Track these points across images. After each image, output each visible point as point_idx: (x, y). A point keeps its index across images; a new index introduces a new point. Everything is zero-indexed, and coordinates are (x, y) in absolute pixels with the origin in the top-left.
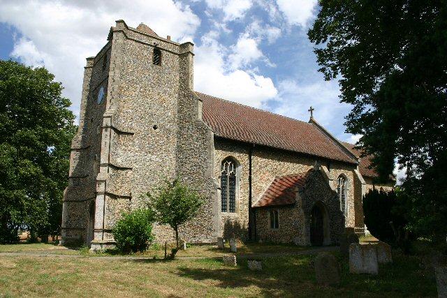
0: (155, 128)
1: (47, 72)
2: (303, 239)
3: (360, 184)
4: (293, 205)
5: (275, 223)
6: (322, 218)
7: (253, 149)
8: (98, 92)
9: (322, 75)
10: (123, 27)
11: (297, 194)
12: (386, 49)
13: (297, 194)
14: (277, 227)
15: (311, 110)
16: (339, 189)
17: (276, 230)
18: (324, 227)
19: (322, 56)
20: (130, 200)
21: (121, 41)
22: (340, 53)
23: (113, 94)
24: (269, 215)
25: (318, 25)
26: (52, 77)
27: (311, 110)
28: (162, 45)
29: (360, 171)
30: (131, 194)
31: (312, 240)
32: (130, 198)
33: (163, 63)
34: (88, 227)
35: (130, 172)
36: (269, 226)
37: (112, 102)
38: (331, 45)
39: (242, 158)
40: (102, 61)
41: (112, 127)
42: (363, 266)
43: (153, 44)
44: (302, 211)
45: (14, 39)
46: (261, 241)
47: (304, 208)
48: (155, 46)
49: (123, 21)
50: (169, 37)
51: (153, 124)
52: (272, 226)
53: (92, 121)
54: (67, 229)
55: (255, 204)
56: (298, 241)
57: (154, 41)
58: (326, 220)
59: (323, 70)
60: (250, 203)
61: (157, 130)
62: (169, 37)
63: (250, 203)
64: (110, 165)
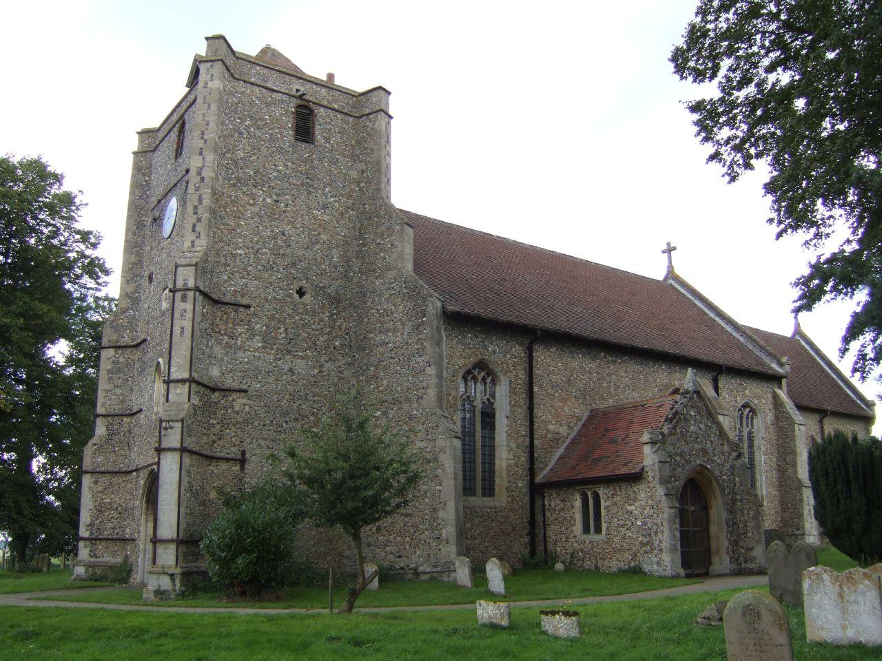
0: (301, 293)
1: (45, 167)
2: (664, 558)
3: (792, 423)
4: (636, 477)
5: (592, 521)
6: (706, 508)
7: (533, 336)
8: (163, 210)
9: (717, 168)
10: (224, 51)
11: (647, 449)
12: (709, 30)
13: (647, 449)
14: (598, 530)
15: (670, 250)
16: (741, 437)
17: (596, 538)
18: (713, 529)
19: (708, 117)
20: (242, 468)
21: (216, 84)
22: (752, 104)
23: (200, 211)
24: (578, 503)
25: (695, 35)
26: (58, 178)
27: (670, 250)
28: (312, 94)
29: (790, 394)
30: (243, 453)
31: (685, 563)
32: (243, 462)
33: (319, 137)
34: (142, 534)
35: (241, 401)
36: (578, 528)
37: (198, 229)
38: (727, 89)
39: (505, 354)
40: (174, 135)
41: (197, 289)
42: (844, 628)
43: (294, 92)
44: (660, 491)
45: (698, 379)
46: (559, 566)
47: (664, 481)
48: (301, 97)
49: (223, 38)
50: (331, 76)
51: (296, 286)
52: (586, 530)
53: (150, 279)
54: (93, 540)
55: (539, 478)
56: (650, 564)
57: (296, 86)
58: (718, 511)
59: (715, 157)
60: (532, 471)
61: (307, 298)
62: (331, 76)
63: (532, 471)
64: (191, 380)
